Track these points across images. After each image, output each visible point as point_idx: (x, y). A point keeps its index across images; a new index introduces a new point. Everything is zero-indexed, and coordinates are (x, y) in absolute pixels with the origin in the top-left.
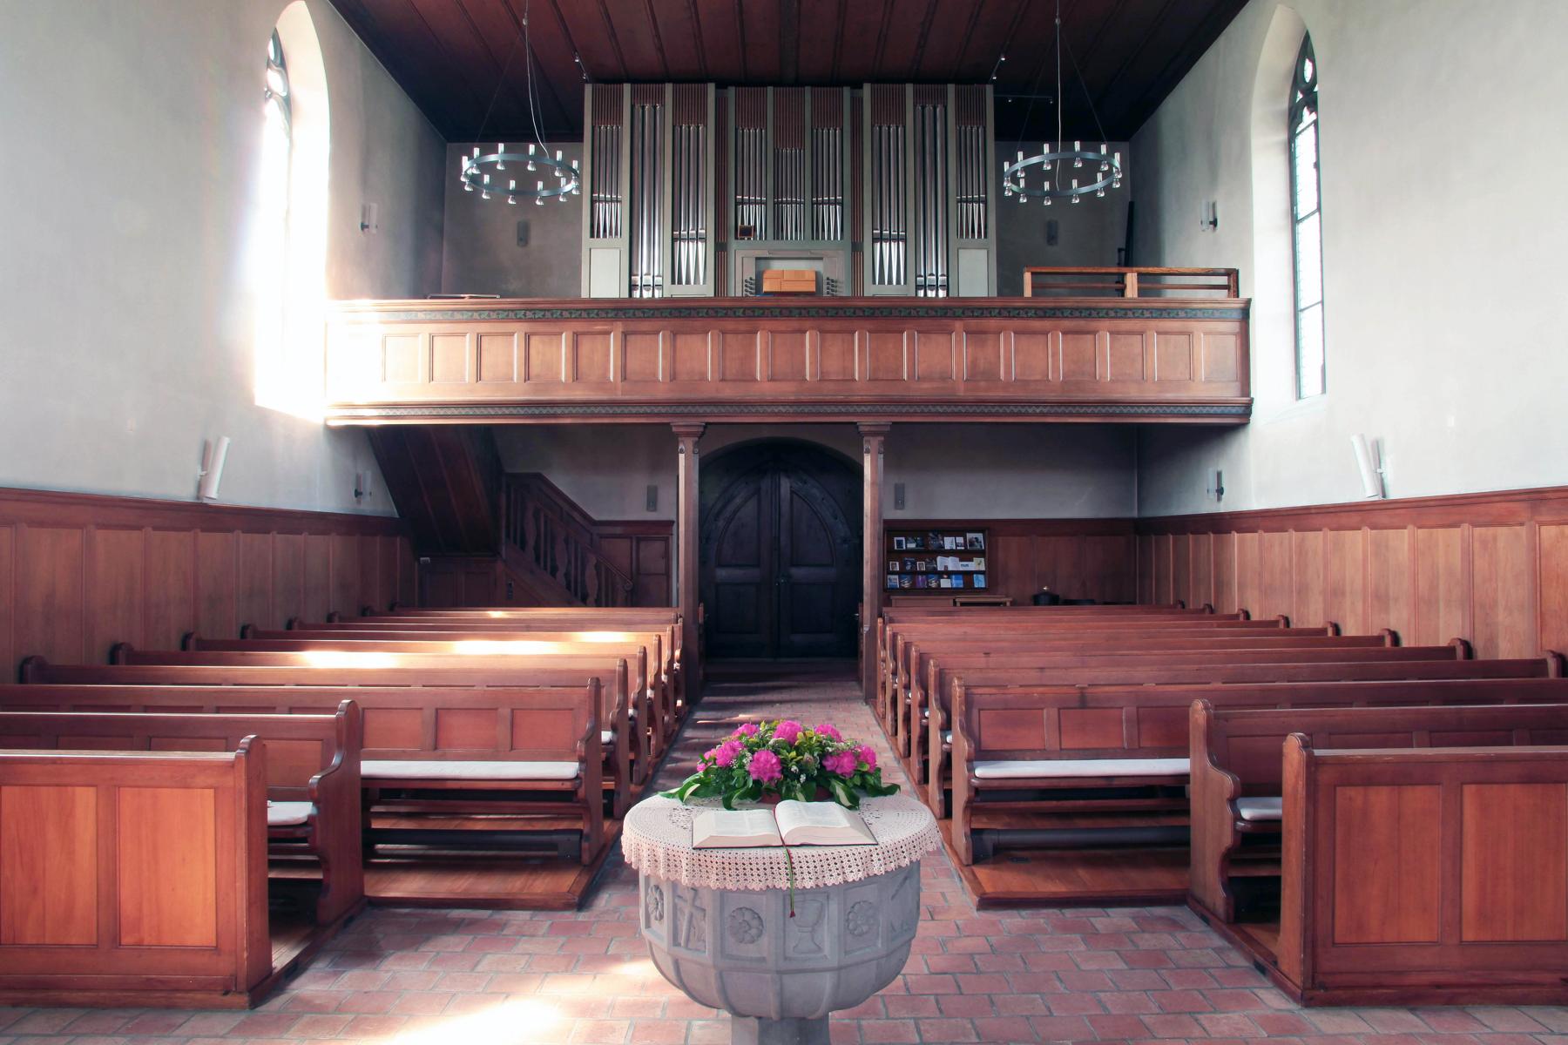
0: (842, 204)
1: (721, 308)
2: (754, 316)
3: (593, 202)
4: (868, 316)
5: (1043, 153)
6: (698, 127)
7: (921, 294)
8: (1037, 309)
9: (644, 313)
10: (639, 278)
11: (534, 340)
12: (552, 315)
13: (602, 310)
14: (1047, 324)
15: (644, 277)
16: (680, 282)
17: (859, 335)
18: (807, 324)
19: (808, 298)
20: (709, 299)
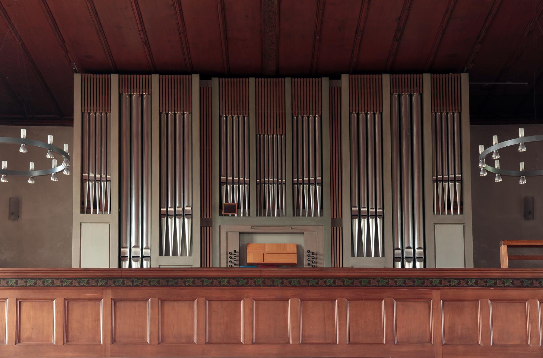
0: (322, 184)
1: (277, 278)
2: (238, 286)
3: (83, 181)
4: (348, 286)
5: (518, 137)
6: (183, 114)
7: (399, 265)
8: (514, 279)
9: (133, 282)
10: (128, 250)
11: (26, 306)
12: (43, 282)
13: (93, 279)
14: (524, 293)
15: (133, 249)
16: (167, 254)
17: (339, 303)
18: (288, 292)
19: (290, 269)
20: (192, 270)
